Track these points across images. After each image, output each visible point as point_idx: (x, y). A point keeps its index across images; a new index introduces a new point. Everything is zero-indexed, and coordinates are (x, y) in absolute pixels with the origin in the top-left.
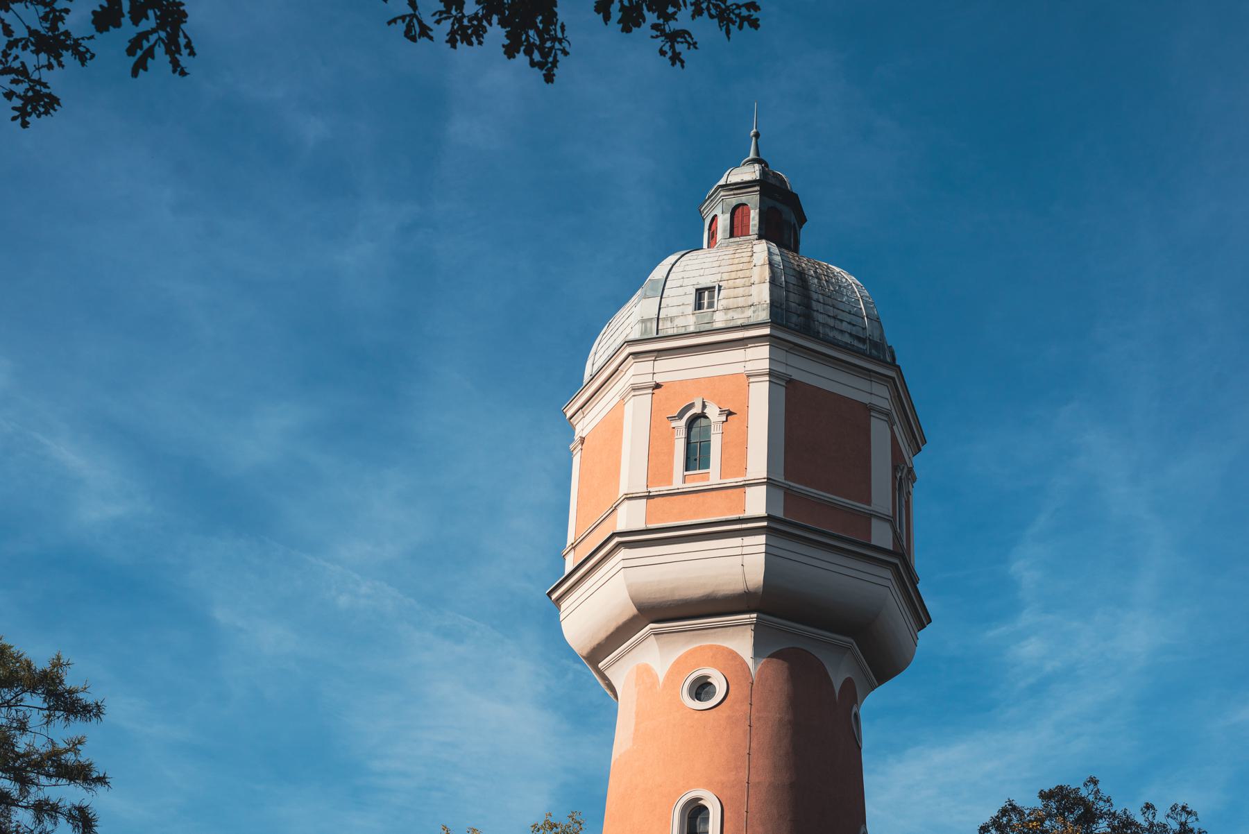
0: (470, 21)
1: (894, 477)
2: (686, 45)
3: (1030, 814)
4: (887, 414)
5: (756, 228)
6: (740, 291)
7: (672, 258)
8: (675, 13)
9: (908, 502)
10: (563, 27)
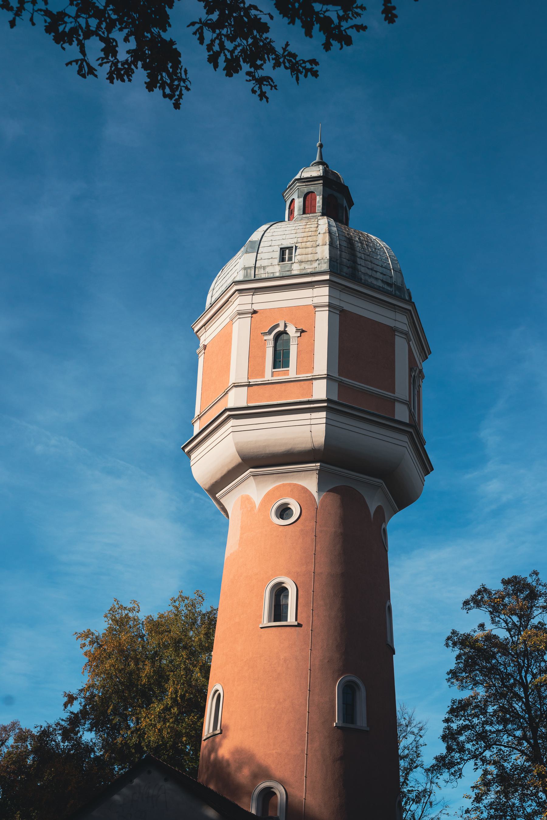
0: (122, 65)
1: (410, 376)
2: (269, 87)
3: (495, 594)
4: (406, 334)
5: (320, 208)
6: (310, 250)
7: (264, 227)
8: (262, 65)
9: (419, 392)
10: (186, 71)
